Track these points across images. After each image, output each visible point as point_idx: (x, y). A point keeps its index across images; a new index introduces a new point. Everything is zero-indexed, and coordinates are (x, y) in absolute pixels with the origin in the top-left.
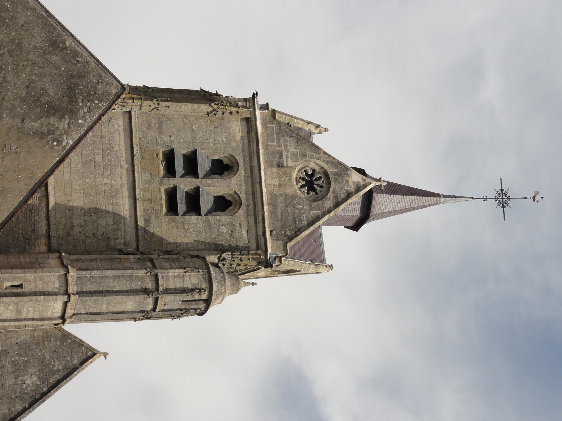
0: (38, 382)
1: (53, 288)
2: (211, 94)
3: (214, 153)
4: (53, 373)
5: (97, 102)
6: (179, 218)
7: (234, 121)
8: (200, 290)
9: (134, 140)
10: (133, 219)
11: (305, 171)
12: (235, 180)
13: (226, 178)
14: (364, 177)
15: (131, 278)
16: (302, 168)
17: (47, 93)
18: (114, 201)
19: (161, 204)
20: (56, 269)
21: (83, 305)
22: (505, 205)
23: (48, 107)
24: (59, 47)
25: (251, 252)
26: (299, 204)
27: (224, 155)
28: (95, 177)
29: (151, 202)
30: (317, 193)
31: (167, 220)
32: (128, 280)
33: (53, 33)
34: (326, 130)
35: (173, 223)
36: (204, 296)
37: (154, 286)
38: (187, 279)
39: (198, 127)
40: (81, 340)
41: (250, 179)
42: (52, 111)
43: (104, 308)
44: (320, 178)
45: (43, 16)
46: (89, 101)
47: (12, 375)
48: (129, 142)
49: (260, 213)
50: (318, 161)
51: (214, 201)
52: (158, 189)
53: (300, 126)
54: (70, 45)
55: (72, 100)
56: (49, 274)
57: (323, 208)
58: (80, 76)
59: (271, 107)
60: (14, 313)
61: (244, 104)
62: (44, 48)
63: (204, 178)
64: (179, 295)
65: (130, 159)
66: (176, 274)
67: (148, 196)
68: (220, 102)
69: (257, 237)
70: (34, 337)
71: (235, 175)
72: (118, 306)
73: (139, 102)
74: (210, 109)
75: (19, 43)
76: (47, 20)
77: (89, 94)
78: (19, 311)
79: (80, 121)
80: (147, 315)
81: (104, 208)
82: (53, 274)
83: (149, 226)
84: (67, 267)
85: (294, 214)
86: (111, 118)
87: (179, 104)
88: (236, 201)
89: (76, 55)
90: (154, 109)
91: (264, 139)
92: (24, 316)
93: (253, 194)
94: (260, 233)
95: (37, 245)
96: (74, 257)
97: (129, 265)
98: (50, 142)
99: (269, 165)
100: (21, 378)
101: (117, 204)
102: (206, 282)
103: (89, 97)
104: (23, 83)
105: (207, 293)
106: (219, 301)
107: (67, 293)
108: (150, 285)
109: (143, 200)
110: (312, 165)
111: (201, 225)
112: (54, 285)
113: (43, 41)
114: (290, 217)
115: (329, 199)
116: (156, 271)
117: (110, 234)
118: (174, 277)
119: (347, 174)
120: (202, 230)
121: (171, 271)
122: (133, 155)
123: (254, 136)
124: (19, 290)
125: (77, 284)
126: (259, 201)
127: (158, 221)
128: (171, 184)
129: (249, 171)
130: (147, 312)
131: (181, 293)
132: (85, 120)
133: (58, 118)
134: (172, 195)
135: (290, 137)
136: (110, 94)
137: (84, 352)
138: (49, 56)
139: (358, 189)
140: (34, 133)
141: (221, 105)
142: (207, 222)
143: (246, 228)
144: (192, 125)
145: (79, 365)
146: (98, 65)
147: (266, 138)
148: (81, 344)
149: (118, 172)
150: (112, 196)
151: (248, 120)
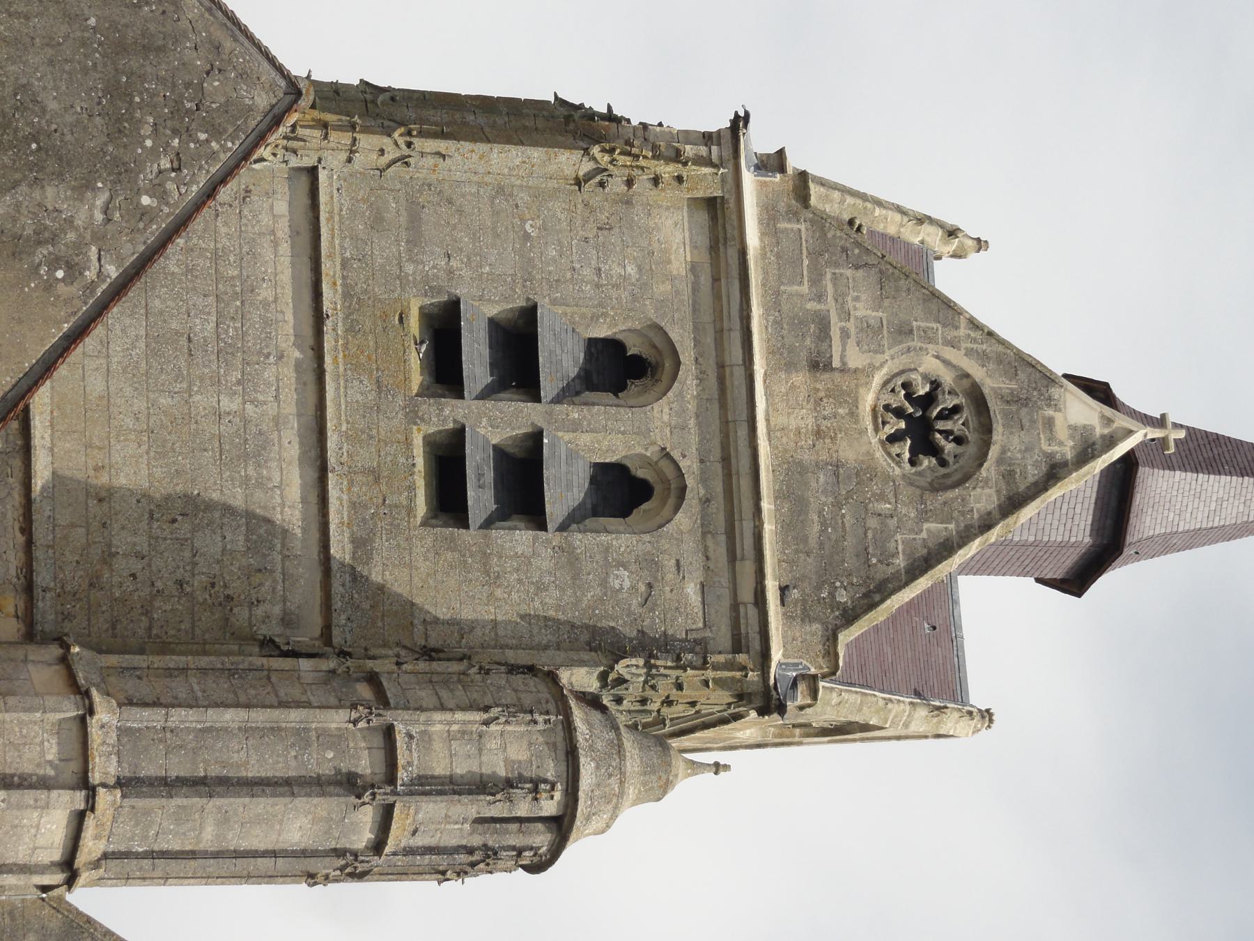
1: (38, 765)
2: (590, 115)
3: (595, 318)
5: (203, 136)
7: (668, 208)
8: (536, 786)
9: (326, 266)
10: (315, 535)
11: (905, 386)
12: (666, 410)
13: (632, 402)
14: (1108, 411)
15: (301, 736)
16: (902, 372)
17: (35, 101)
18: (251, 471)
19: (412, 488)
20: (50, 701)
21: (137, 825)
23: (39, 149)
25: (713, 659)
26: (881, 497)
27: (629, 325)
29: (377, 480)
30: (943, 463)
31: (429, 541)
32: (293, 745)
34: (980, 244)
35: (449, 555)
36: (550, 806)
37: (380, 768)
38: (493, 744)
39: (544, 227)
42: (52, 165)
43: (208, 838)
44: (956, 410)
46: (176, 132)
48: (307, 275)
49: (748, 526)
50: (949, 354)
51: (593, 480)
52: (401, 437)
53: (892, 230)
56: (25, 717)
57: (963, 513)
58: (150, 47)
59: (795, 162)
61: (703, 150)
63: (557, 400)
64: (465, 799)
65: (308, 331)
66: (455, 728)
67: (366, 457)
68: (619, 145)
69: (735, 606)
72: (257, 831)
73: (346, 138)
74: (586, 167)
77: (177, 110)
79: (146, 200)
81: (215, 496)
82: (38, 715)
84: (87, 694)
85: (861, 531)
86: (248, 191)
87: (482, 147)
88: (665, 481)
90: (394, 162)
91: (765, 273)
93: (726, 460)
94: (747, 595)
96: (113, 660)
97: (295, 693)
98: (43, 270)
99: (783, 361)
101: (260, 484)
102: (556, 759)
105: (558, 795)
106: (601, 825)
107: (84, 783)
108: (366, 763)
110: (929, 364)
111: (545, 561)
112: (42, 753)
114: (849, 543)
115: (986, 481)
116: (389, 716)
117: (236, 587)
118: (450, 737)
119: (1050, 398)
120: (546, 579)
121: (438, 716)
122: (319, 318)
125: (118, 754)
126: (745, 483)
127: (398, 545)
128: (445, 420)
130: (355, 855)
131: (470, 793)
132: (163, 196)
133: (73, 189)
136: (250, 109)
139: (1086, 454)
141: (622, 153)
144: (524, 221)
146: (209, 10)
149: (269, 374)
150: (246, 456)
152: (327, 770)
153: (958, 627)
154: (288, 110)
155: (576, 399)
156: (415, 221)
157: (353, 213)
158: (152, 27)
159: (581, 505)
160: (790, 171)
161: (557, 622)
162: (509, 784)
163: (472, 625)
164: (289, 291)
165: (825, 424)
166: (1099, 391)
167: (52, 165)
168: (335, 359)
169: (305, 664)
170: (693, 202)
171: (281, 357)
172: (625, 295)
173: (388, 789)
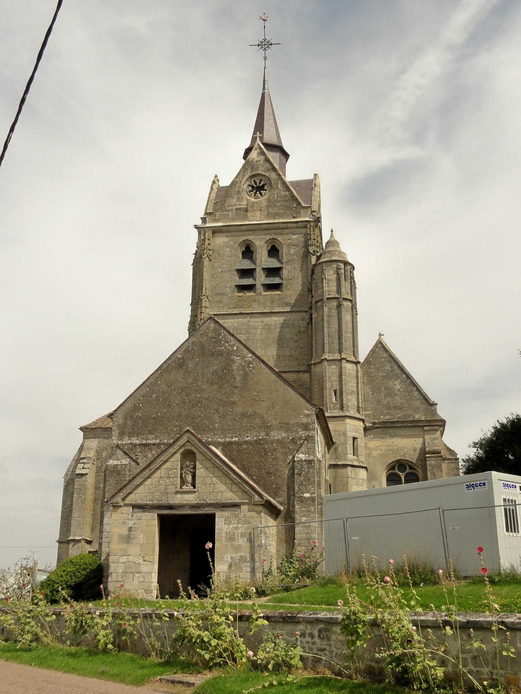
0: (399, 380)
1: (337, 369)
2: (195, 258)
3: (238, 257)
4: (393, 370)
5: (221, 337)
6: (285, 283)
8: (338, 269)
9: (230, 312)
10: (285, 314)
11: (250, 192)
13: (255, 249)
14: (254, 149)
15: (329, 316)
16: (247, 193)
17: (215, 371)
18: (272, 327)
19: (275, 294)
20: (324, 367)
22: (270, 43)
24: (182, 362)
25: (309, 232)
26: (274, 197)
27: (239, 250)
28: (256, 340)
30: (266, 184)
31: (286, 291)
33: (173, 366)
34: (216, 176)
35: (288, 287)
36: (342, 266)
37: (336, 300)
38: (330, 277)
39: (220, 268)
40: (370, 351)
41: (256, 232)
42: (229, 367)
43: (350, 335)
44: (254, 181)
45: (161, 373)
46: (220, 342)
47: (394, 398)
48: (232, 316)
49: (281, 225)
51: (271, 257)
53: (215, 195)
54: (181, 354)
55: (220, 354)
56: (327, 372)
57: (277, 180)
58: (203, 348)
60: (353, 396)
61: (202, 235)
62: (184, 372)
63: (256, 265)
64: (341, 283)
65: (243, 316)
67: (269, 304)
68: (202, 252)
69: (297, 228)
70: (368, 382)
71: (253, 243)
72: (348, 325)
73: (203, 308)
74: (207, 259)
75: (181, 389)
76: (164, 370)
77: (216, 342)
78: (352, 393)
79: (235, 348)
80: (354, 307)
81: (278, 334)
83: (290, 303)
84: (322, 360)
87: (204, 281)
88: (271, 242)
89: (187, 351)
90: (208, 299)
91: (227, 221)
92: (355, 389)
93: (267, 230)
94: (295, 225)
95: (304, 380)
96: (314, 355)
97: (320, 318)
99: (246, 218)
100: (396, 392)
101: (275, 326)
102: (333, 265)
103: (218, 342)
104: (208, 387)
105: (340, 264)
106: (345, 255)
108: (334, 303)
109: (272, 307)
110: (245, 187)
111: (289, 267)
112: (334, 368)
113: (178, 373)
114: (284, 204)
115: (270, 175)
116: (325, 299)
117: (296, 330)
118: (328, 286)
119: (252, 161)
120: (293, 267)
121: (324, 289)
122: (241, 314)
123: (225, 228)
124: (338, 392)
125: (334, 353)
126: (272, 226)
128: (260, 288)
129: (250, 232)
130: (352, 305)
131: (340, 282)
132: (234, 345)
134: (269, 287)
135: (225, 202)
136: (214, 327)
137: (379, 349)
138: (189, 369)
139: (262, 153)
140: (244, 380)
141: (204, 251)
142: (287, 263)
143: (291, 235)
144: (218, 272)
145: (387, 353)
146: (194, 336)
147: (227, 220)
148: (373, 351)
149: (252, 324)
150: (270, 328)
151: (214, 232)
152: (336, 311)
153: (297, 181)
154: (214, 319)
155: (255, 261)
156: (220, 294)
157: (219, 307)
158: (199, 348)
159: (277, 260)
160: (206, 216)
161: (302, 264)
162: (338, 274)
163: (303, 282)
164: (235, 320)
165: (259, 209)
166: (248, 151)
167: (229, 367)
168: (249, 310)
169: (314, 316)
170: (213, 237)
171: (249, 322)
172: (233, 251)
173: (340, 299)
